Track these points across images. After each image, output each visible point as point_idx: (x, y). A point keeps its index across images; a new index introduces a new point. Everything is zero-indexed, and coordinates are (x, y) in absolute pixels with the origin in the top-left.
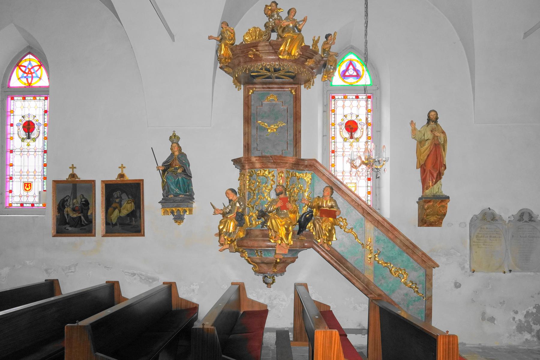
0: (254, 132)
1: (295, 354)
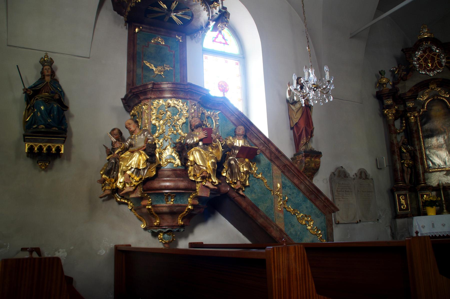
0: (139, 71)
1: (294, 5)
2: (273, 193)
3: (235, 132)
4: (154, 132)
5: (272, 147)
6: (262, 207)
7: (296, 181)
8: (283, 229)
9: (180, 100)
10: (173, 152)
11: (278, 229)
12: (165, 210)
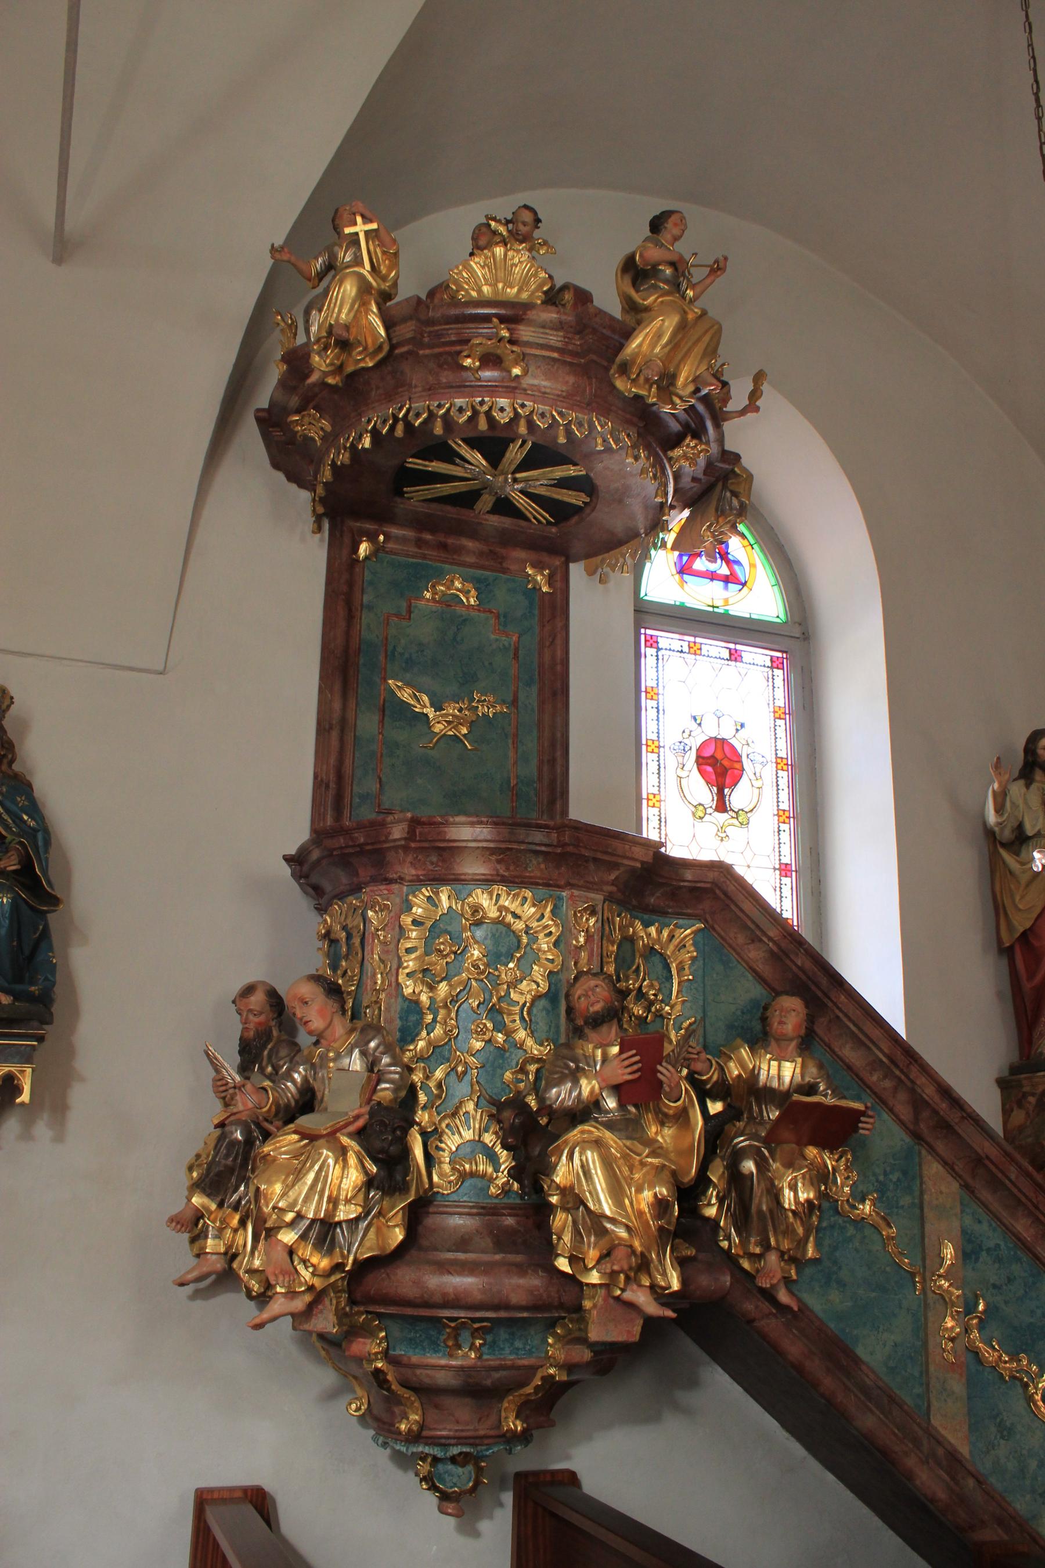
0: (367, 724)
2: (924, 1281)
3: (764, 1020)
4: (408, 1036)
5: (922, 1080)
6: (873, 1350)
7: (1022, 1226)
8: (964, 1450)
9: (528, 894)
10: (486, 1130)
11: (940, 1452)
12: (442, 1378)
